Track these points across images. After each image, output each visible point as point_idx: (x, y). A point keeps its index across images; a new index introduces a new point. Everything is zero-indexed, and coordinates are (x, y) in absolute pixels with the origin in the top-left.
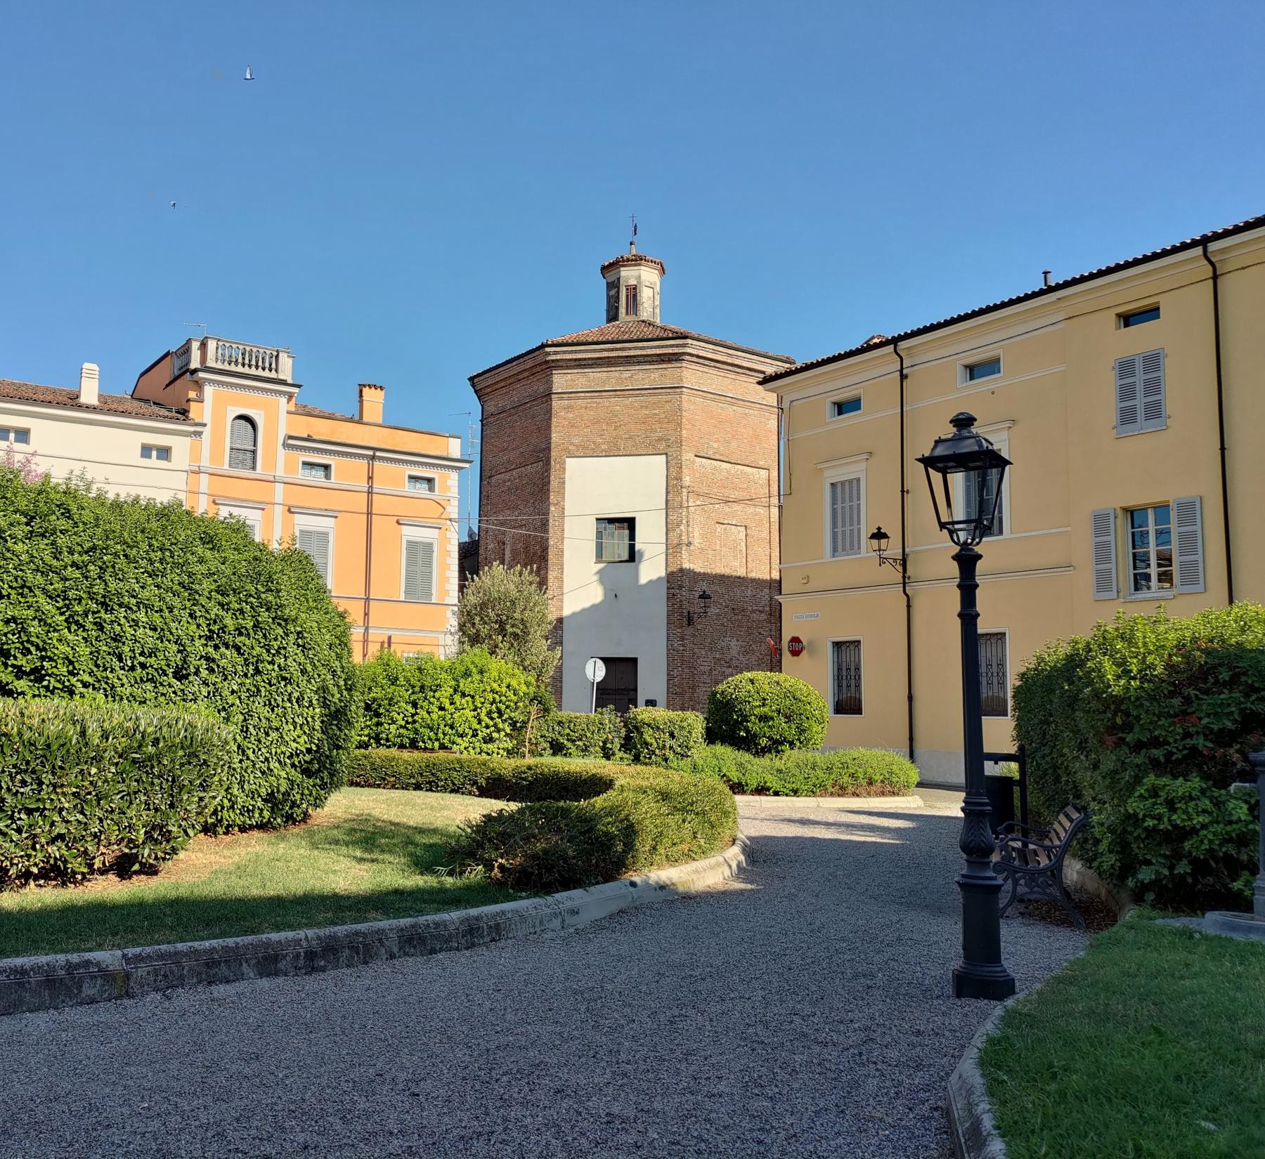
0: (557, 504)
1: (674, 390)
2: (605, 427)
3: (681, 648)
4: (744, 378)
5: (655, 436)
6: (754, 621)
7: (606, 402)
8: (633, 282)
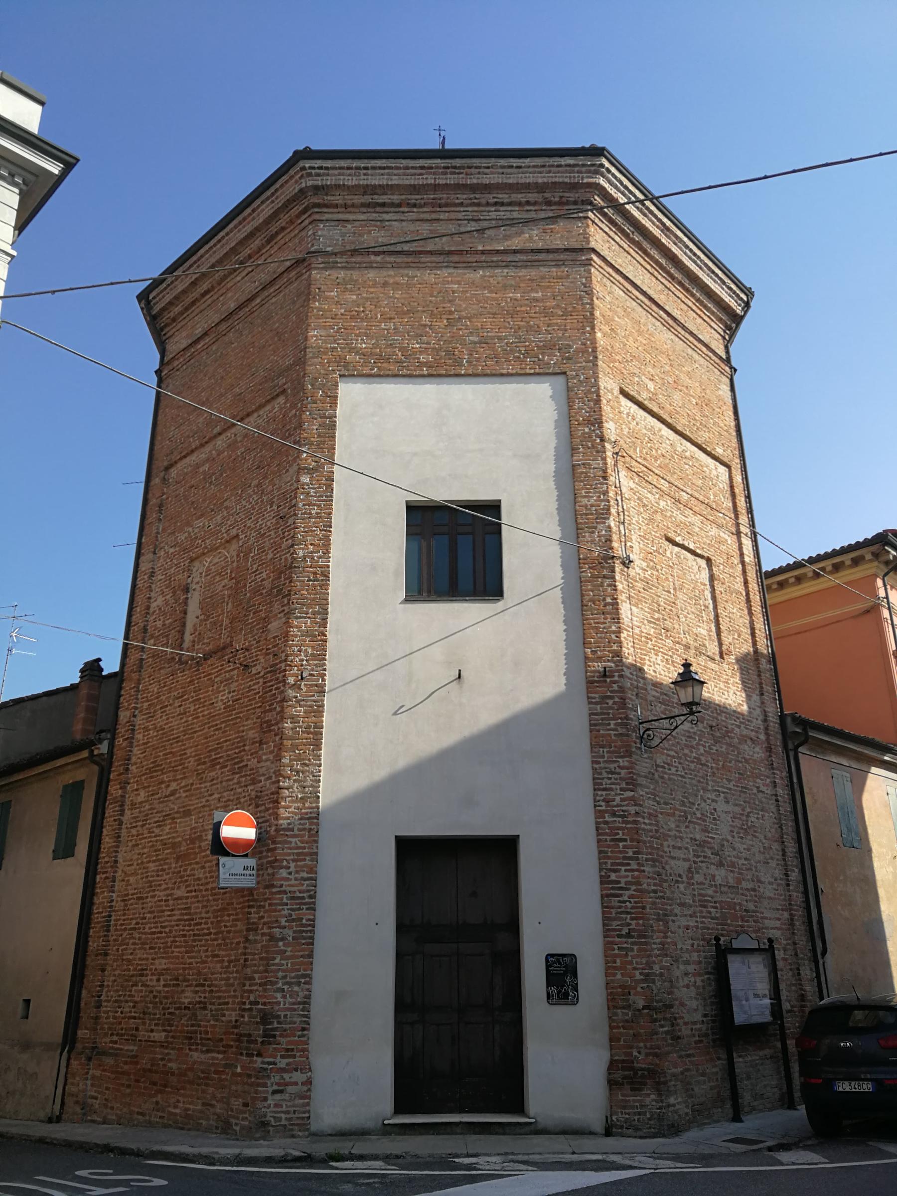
0: (315, 470)
2: (425, 320)
5: (536, 340)
6: (747, 761)
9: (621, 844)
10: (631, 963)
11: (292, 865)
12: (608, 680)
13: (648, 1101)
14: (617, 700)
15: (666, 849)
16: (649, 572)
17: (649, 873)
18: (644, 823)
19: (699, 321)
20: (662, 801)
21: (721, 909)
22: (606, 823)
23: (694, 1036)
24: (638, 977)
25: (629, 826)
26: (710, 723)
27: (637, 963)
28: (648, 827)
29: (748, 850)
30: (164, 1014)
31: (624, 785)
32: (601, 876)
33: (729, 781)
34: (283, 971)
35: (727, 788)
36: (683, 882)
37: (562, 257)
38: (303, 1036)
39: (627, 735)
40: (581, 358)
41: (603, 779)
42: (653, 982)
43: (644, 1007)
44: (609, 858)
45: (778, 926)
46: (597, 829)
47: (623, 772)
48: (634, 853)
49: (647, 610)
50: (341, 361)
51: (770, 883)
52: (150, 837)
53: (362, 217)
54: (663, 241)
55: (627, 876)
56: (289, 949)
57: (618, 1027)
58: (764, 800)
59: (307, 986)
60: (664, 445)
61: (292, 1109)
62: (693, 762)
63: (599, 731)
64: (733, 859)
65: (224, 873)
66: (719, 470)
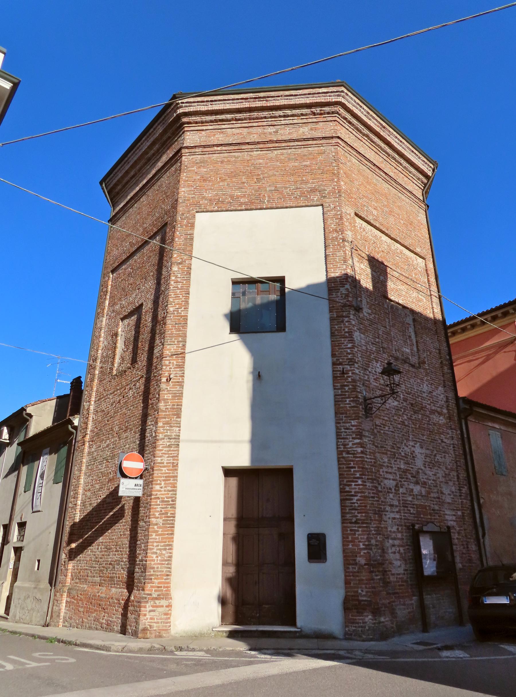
2: (244, 180)
3: (359, 450)
6: (435, 424)
9: (352, 470)
10: (358, 538)
11: (163, 483)
12: (346, 376)
13: (367, 619)
14: (350, 387)
15: (381, 473)
16: (373, 316)
17: (369, 486)
19: (406, 179)
20: (379, 446)
21: (417, 508)
22: (343, 458)
23: (398, 582)
24: (362, 546)
25: (357, 459)
26: (411, 402)
27: (361, 538)
28: (369, 460)
29: (435, 475)
30: (100, 567)
31: (354, 436)
32: (341, 489)
33: (423, 435)
34: (157, 542)
35: (421, 439)
36: (392, 493)
37: (321, 142)
38: (167, 579)
39: (357, 407)
41: (342, 432)
42: (371, 549)
43: (365, 564)
44: (345, 478)
45: (454, 519)
46: (338, 461)
47: (354, 428)
48: (360, 475)
49: (371, 336)
50: (197, 204)
51: (449, 495)
52: (97, 470)
53: (211, 127)
54: (381, 134)
55: (355, 488)
56: (161, 530)
57: (350, 576)
58: (446, 447)
59: (170, 551)
60: (383, 245)
61: (160, 621)
62: (399, 424)
63: (340, 405)
64: (425, 480)
65: (123, 488)
66: (418, 261)
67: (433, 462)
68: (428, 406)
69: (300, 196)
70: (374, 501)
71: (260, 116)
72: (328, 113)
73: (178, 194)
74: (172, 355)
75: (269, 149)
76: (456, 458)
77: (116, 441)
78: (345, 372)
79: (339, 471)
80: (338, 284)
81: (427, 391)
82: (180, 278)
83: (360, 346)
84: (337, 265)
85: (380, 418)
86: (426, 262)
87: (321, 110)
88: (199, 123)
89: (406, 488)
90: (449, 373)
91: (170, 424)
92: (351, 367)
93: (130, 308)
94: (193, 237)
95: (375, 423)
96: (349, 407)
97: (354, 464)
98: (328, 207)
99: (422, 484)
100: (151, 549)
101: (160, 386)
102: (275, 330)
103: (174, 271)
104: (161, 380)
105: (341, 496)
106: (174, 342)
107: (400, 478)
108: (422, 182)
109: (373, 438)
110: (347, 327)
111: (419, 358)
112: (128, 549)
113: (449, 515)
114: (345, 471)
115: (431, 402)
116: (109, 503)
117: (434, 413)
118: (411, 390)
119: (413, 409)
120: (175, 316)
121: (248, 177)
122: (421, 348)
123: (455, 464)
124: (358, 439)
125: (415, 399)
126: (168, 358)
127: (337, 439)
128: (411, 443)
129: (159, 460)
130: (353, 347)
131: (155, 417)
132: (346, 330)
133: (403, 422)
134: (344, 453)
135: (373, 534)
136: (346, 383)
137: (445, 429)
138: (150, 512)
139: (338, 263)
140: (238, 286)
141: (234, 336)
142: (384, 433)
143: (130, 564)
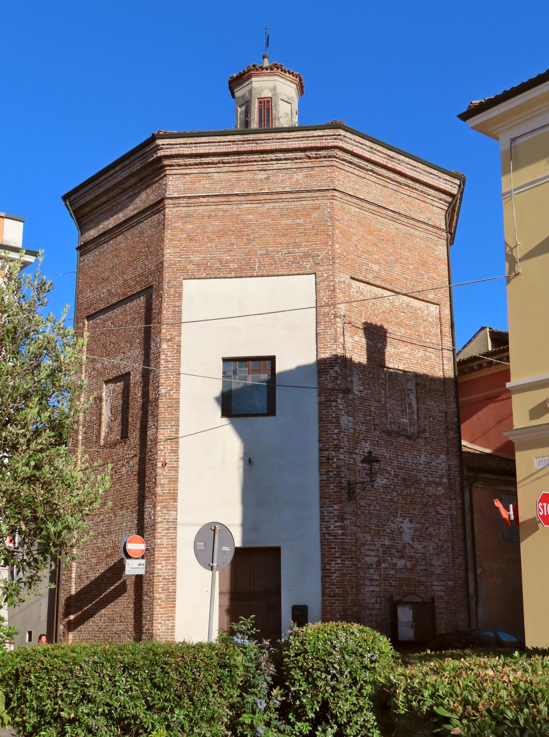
0: (169, 340)
1: (323, 193)
2: (234, 241)
3: (340, 532)
4: (406, 191)
7: (233, 209)
8: (267, 94)
9: (333, 550)
10: (335, 609)
11: (164, 562)
12: (331, 462)
14: (335, 472)
16: (365, 392)
17: (348, 564)
18: (347, 539)
22: (326, 539)
26: (404, 477)
31: (336, 519)
32: (322, 567)
33: (414, 509)
34: (161, 614)
35: (412, 514)
40: (325, 263)
44: (326, 557)
46: (321, 542)
47: (336, 512)
48: (340, 555)
49: (361, 416)
50: (183, 270)
55: (335, 567)
56: (164, 604)
59: (173, 621)
60: (385, 304)
62: (387, 501)
63: (324, 490)
64: (412, 554)
66: (430, 309)
67: (424, 535)
68: (424, 479)
69: (293, 263)
70: (352, 577)
71: (249, 160)
72: (325, 157)
73: (163, 256)
74: (166, 440)
75: (259, 202)
76: (452, 529)
77: (111, 517)
78: (330, 457)
79: (322, 551)
80: (327, 366)
81: (424, 462)
82: (170, 357)
83: (347, 430)
84: (327, 345)
85: (365, 499)
86: (440, 309)
87: (316, 154)
88: (183, 165)
89: (389, 563)
90: (455, 438)
91: (168, 508)
92: (336, 453)
93: (115, 373)
94: (181, 309)
95: (360, 504)
96: (333, 492)
97: (334, 545)
98: (320, 277)
99: (408, 558)
100: (156, 620)
101: (156, 471)
102: (266, 412)
103: (164, 349)
104: (156, 465)
105: (322, 573)
106: (167, 426)
107: (383, 554)
108: (446, 202)
109: (356, 520)
110: (334, 412)
111: (419, 427)
112: (133, 620)
113: (437, 586)
114: (327, 551)
115: (428, 474)
116: (109, 578)
117: (431, 485)
118: (405, 465)
119: (405, 484)
120: (168, 399)
121: (237, 237)
122: (422, 414)
123: (451, 535)
124: (340, 522)
125: (409, 474)
126: (162, 443)
127: (321, 522)
128: (400, 519)
129: (159, 541)
130: (338, 433)
131: (152, 501)
132: (334, 415)
133: (392, 500)
134: (326, 535)
135: (349, 606)
136: (330, 469)
137: (442, 500)
138: (153, 588)
139: (329, 342)
140: (228, 363)
141: (225, 421)
142: (369, 513)
143: (136, 633)
